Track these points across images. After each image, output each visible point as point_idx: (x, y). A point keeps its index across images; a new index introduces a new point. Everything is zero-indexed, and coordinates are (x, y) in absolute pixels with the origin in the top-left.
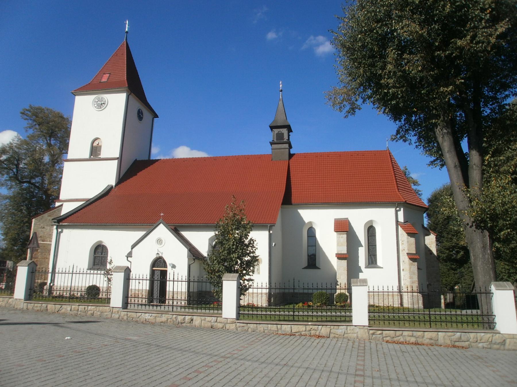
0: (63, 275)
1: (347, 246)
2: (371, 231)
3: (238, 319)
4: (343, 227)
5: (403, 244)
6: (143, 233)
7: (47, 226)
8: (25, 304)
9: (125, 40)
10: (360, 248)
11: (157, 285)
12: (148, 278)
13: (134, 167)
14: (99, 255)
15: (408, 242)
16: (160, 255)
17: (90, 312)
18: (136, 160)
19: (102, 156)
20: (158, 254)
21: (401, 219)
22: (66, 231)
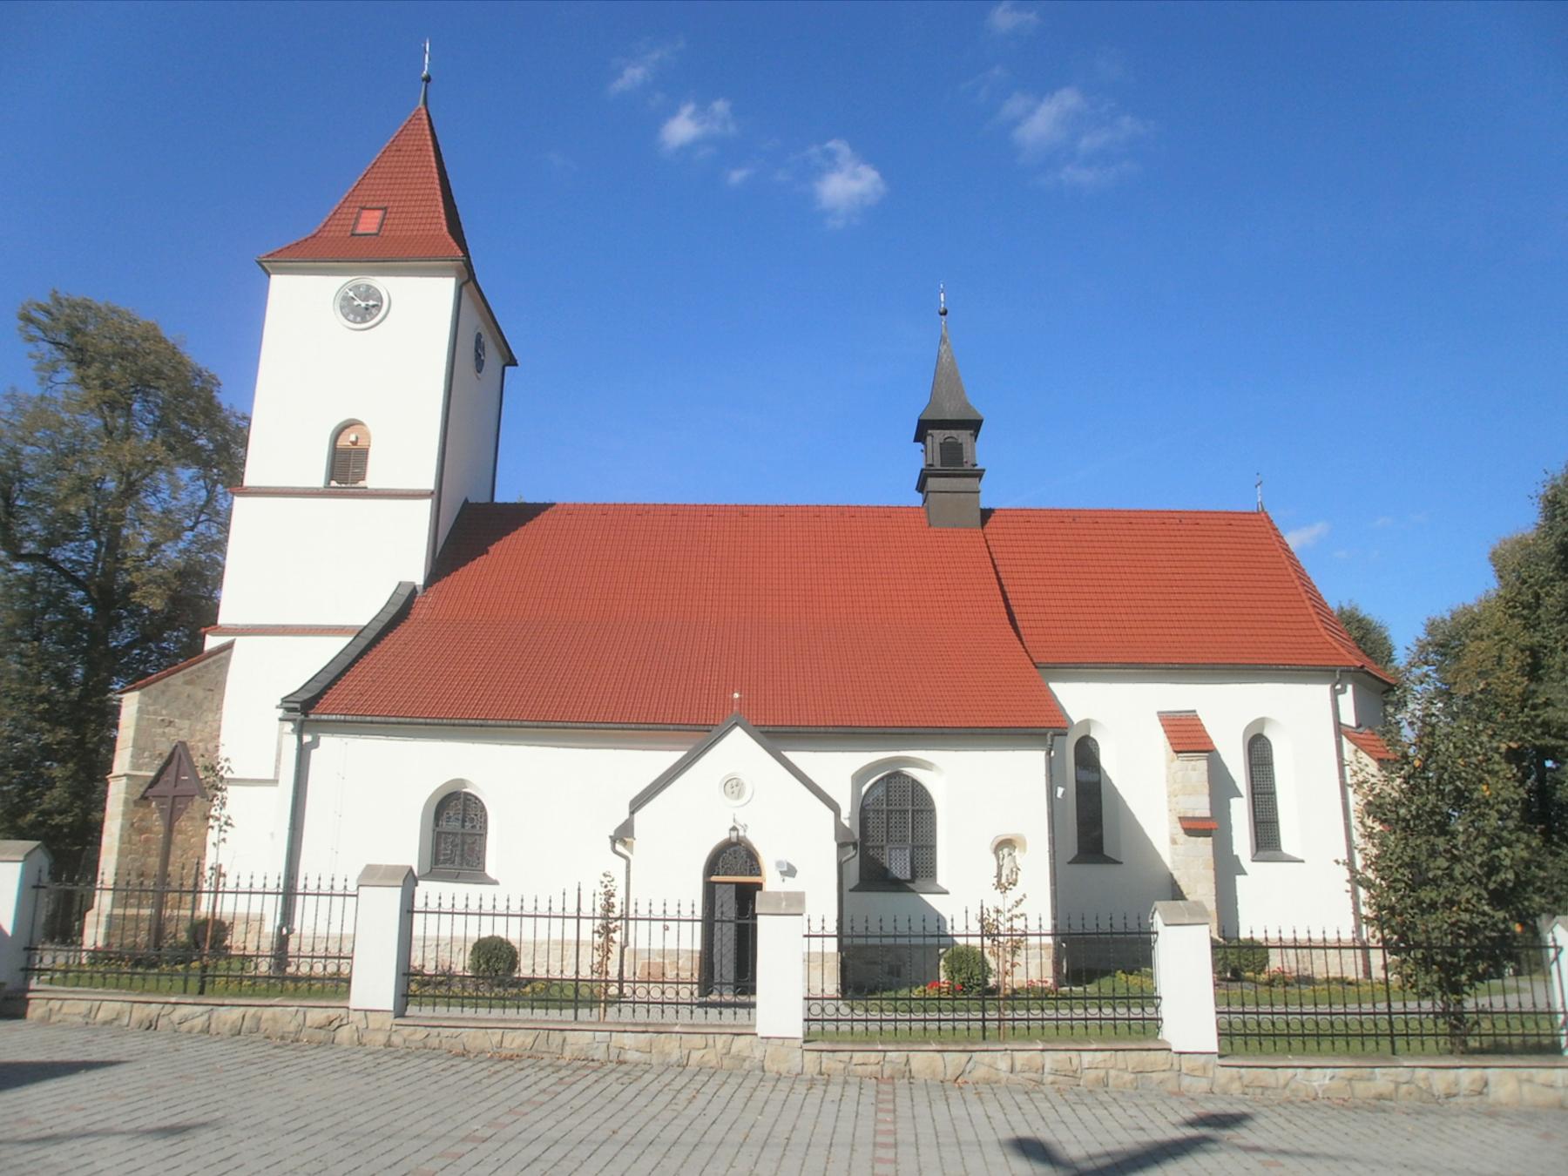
0: (324, 900)
1: (1210, 795)
2: (1258, 749)
3: (400, 1012)
4: (1186, 736)
6: (674, 757)
7: (181, 716)
8: (808, 1055)
9: (421, 104)
10: (1234, 801)
12: (699, 914)
13: (472, 529)
17: (1092, 1074)
19: (372, 481)
21: (1349, 717)
22: (327, 741)
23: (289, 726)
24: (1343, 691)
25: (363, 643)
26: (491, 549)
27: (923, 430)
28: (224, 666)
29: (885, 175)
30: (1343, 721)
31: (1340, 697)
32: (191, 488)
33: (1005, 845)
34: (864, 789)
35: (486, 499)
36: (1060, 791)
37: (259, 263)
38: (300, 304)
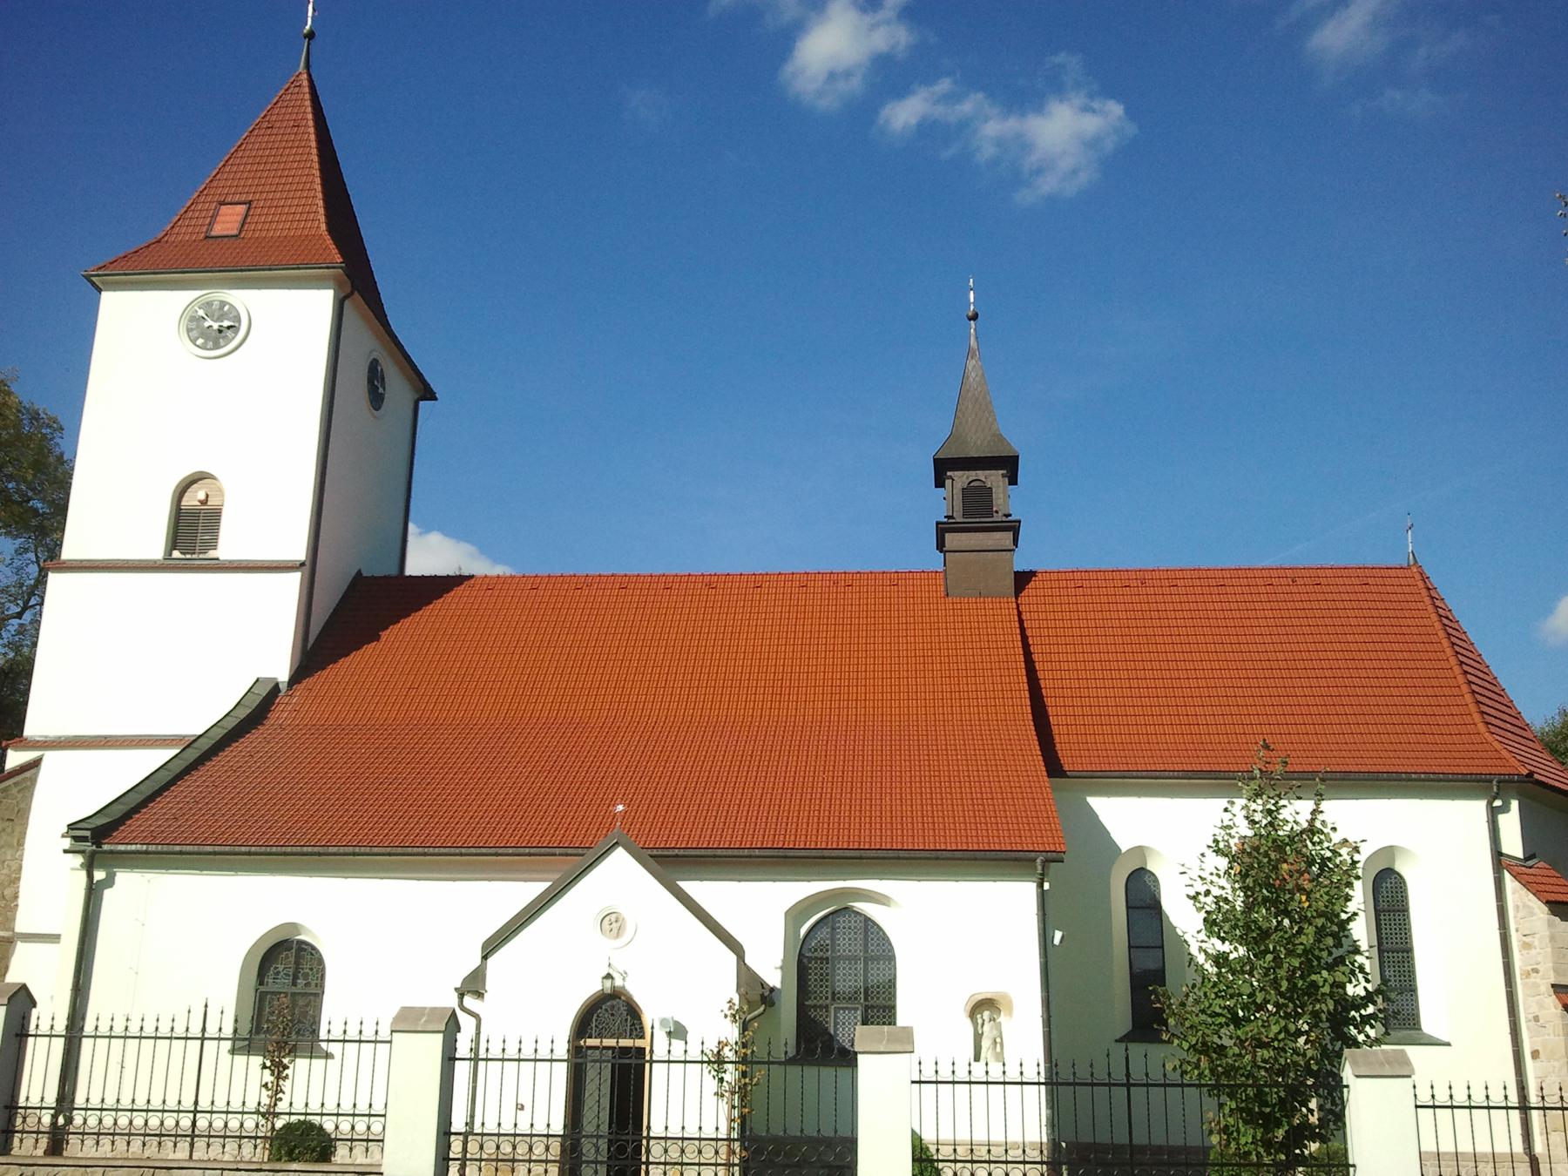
5: (1527, 946)
6: (533, 889)
11: (597, 1114)
13: (357, 607)
14: (279, 983)
15: (1552, 938)
16: (618, 982)
18: (359, 573)
19: (225, 550)
20: (609, 976)
21: (1513, 844)
22: (127, 880)
23: (79, 860)
24: (1505, 809)
25: (193, 755)
26: (384, 635)
27: (942, 468)
28: (28, 789)
29: (1131, 113)
30: (1504, 850)
31: (1501, 818)
32: (17, 563)
33: (984, 1007)
34: (803, 930)
35: (394, 571)
36: (1058, 935)
37: (88, 278)
38: (136, 327)
